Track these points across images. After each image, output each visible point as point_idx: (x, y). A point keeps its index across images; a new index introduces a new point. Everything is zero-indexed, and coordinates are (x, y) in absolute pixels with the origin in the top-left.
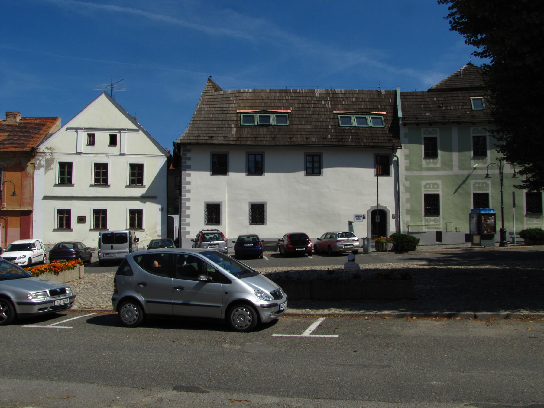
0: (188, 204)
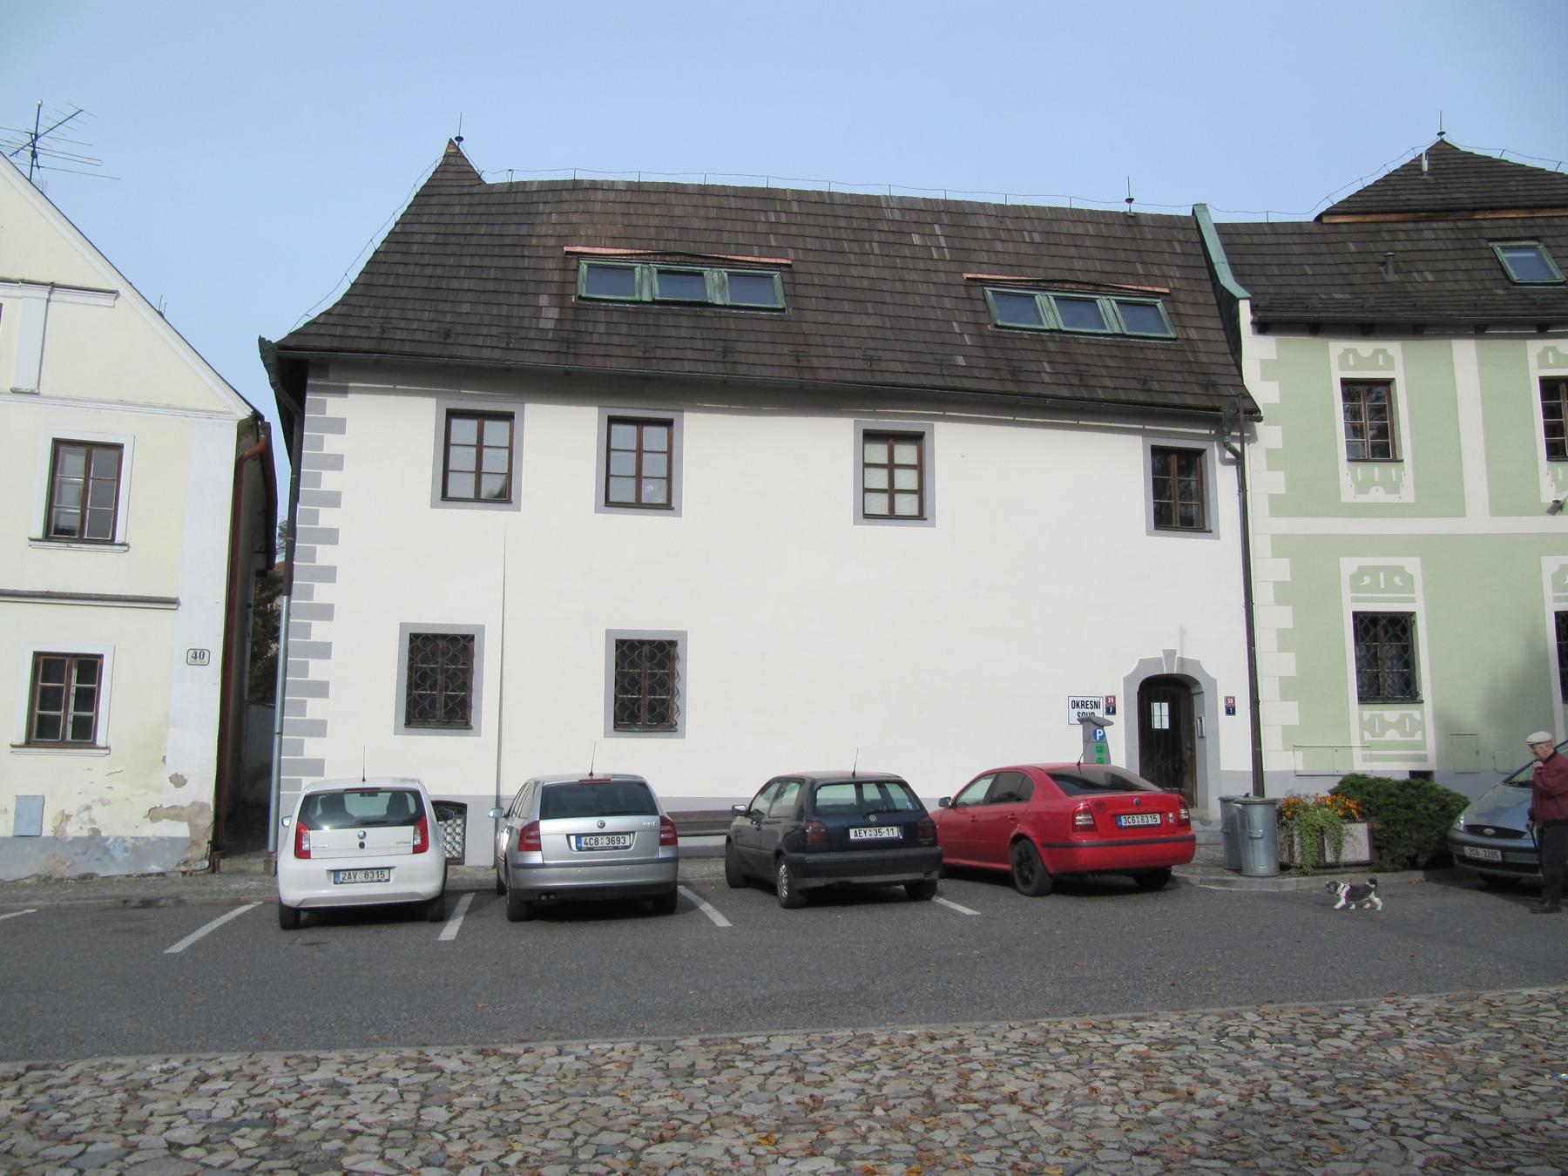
0: (325, 555)
